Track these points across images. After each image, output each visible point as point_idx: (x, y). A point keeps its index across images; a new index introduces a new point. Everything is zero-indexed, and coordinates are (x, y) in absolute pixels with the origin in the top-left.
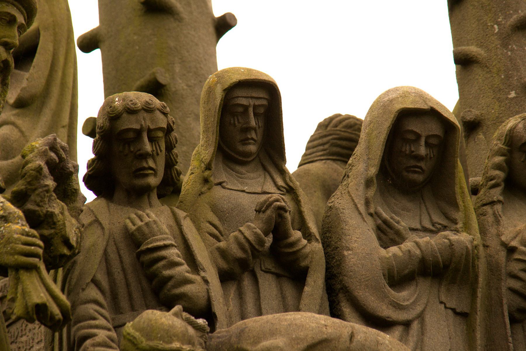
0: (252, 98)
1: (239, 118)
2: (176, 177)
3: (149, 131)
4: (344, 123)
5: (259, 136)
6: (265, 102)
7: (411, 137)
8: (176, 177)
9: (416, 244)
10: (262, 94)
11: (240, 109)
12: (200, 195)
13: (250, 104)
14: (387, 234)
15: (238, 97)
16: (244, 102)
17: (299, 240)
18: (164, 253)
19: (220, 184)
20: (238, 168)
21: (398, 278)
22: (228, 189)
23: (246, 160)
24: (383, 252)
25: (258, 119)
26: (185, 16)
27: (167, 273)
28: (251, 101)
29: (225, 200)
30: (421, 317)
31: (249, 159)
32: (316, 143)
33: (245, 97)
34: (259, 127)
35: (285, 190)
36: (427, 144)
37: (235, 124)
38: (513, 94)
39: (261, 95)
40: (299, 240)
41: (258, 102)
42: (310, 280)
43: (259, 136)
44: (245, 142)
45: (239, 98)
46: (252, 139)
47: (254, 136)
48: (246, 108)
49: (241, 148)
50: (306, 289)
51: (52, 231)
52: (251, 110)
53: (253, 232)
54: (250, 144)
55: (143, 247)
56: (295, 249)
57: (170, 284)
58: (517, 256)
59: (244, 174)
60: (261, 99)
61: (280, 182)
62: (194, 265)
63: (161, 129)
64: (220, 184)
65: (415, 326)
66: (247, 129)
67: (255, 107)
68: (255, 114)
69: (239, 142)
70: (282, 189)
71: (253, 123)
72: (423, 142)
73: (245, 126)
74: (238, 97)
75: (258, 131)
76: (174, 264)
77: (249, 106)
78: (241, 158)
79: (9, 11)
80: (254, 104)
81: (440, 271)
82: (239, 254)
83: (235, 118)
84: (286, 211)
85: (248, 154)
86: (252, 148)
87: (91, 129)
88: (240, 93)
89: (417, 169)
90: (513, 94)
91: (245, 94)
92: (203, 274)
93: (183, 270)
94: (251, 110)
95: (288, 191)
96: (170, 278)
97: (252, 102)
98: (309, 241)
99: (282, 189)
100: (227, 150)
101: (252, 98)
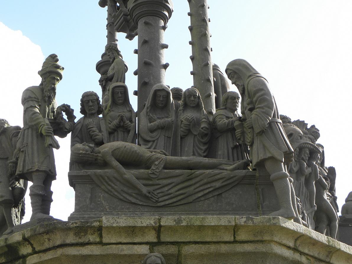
3: (91, 100)
4: (175, 90)
7: (159, 96)
9: (157, 122)
10: (122, 88)
11: (117, 93)
14: (151, 120)
16: (118, 91)
17: (128, 123)
18: (92, 129)
19: (113, 111)
21: (152, 131)
24: (149, 125)
26: (154, 65)
27: (93, 133)
30: (158, 139)
38: (202, 82)
40: (128, 123)
42: (131, 133)
48: (118, 92)
50: (129, 135)
51: (63, 126)
52: (120, 93)
55: (89, 127)
57: (93, 136)
58: (183, 123)
62: (100, 131)
63: (95, 99)
64: (113, 111)
65: (156, 141)
68: (121, 93)
72: (162, 97)
76: (94, 131)
79: (53, 76)
81: (162, 128)
82: (114, 128)
84: (124, 117)
87: (136, 93)
90: (202, 82)
92: (103, 133)
93: (97, 132)
94: (120, 93)
96: (93, 135)
97: (120, 91)
98: (132, 123)
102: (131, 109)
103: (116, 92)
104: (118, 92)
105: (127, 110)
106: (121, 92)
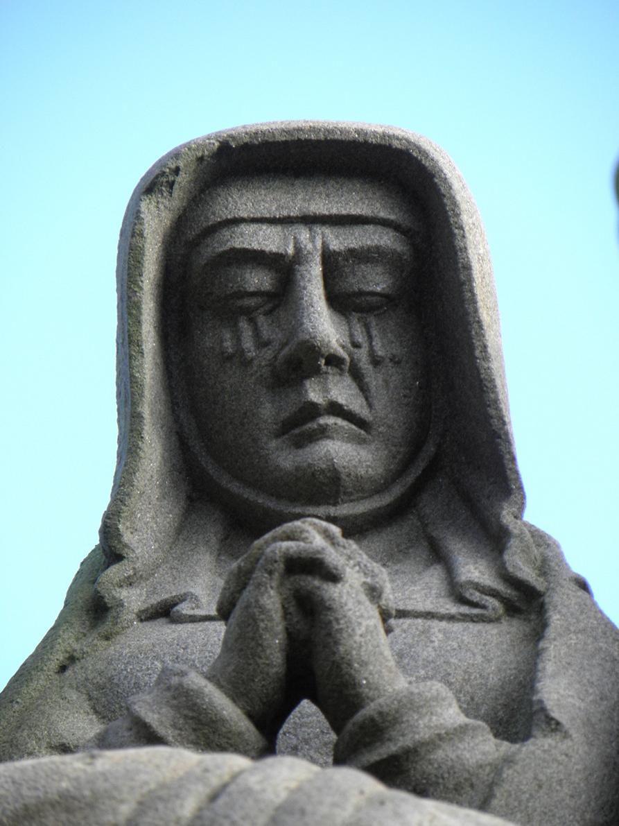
0: (310, 220)
1: (261, 319)
11: (258, 280)
12: (63, 669)
13: (298, 250)
16: (268, 240)
22: (193, 619)
25: (367, 327)
28: (304, 234)
29: (156, 658)
33: (272, 221)
34: (376, 362)
35: (492, 602)
36: (339, 301)
37: (240, 352)
41: (339, 240)
43: (378, 405)
44: (302, 425)
46: (335, 409)
47: (342, 391)
48: (285, 269)
49: (286, 459)
53: (169, 689)
54: (323, 433)
56: (391, 748)
60: (360, 220)
66: (306, 360)
69: (277, 436)
71: (326, 327)
75: (374, 379)
77: (299, 257)
83: (244, 324)
84: (333, 577)
86: (341, 451)
88: (243, 201)
95: (512, 610)
97: (312, 241)
99: (476, 596)
100: (235, 487)
101: (310, 220)
102: (527, 573)
103: (238, 338)
104: (285, 269)
105: (457, 593)
106: (330, 261)
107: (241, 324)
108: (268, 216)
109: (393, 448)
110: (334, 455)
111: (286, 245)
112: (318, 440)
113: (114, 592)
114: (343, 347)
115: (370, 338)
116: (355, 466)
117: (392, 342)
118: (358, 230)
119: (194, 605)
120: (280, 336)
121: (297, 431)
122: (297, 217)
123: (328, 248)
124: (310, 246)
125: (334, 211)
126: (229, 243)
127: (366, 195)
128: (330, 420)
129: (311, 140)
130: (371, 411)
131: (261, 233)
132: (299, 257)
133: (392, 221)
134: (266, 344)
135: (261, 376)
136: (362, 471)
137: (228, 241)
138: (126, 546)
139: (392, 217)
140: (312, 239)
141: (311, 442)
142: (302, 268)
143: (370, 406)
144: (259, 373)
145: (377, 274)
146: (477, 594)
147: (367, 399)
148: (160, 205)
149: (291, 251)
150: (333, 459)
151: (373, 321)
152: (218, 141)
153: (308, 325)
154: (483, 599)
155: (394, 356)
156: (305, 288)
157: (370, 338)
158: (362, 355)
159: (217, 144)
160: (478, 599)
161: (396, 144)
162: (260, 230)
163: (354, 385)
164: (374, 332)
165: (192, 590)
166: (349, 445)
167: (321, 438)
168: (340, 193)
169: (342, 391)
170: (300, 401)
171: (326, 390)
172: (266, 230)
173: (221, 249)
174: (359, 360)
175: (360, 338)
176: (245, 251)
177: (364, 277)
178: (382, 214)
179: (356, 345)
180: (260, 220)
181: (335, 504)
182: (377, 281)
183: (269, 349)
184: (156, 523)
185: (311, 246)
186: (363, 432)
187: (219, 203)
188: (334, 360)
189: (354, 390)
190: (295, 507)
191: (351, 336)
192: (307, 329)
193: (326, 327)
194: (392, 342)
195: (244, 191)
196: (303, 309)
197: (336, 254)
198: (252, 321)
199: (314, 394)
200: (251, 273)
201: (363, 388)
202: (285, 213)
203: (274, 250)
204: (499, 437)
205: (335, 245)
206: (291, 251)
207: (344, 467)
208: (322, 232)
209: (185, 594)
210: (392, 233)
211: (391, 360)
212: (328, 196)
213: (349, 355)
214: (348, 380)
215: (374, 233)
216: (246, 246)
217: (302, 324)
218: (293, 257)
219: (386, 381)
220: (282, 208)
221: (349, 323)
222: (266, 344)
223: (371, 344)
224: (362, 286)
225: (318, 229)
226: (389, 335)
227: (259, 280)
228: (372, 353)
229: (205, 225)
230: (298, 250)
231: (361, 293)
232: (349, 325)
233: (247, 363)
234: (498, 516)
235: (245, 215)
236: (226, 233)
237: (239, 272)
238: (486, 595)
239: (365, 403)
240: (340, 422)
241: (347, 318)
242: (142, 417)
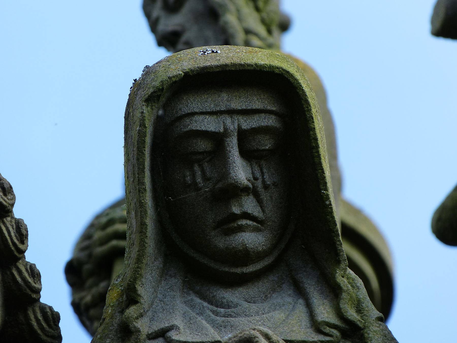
0: (231, 112)
1: (207, 166)
2: (42, 329)
5: (269, 207)
6: (269, 121)
8: (42, 329)
11: (203, 145)
13: (226, 129)
15: (193, 114)
16: (210, 124)
20: (228, 295)
23: (239, 270)
28: (228, 121)
31: (251, 269)
32: (49, 313)
34: (266, 187)
35: (335, 332)
36: (246, 154)
39: (257, 104)
41: (248, 123)
44: (229, 224)
45: (196, 118)
46: (246, 216)
47: (249, 205)
48: (218, 140)
49: (221, 242)
54: (241, 229)
59: (236, 306)
60: (259, 111)
61: (325, 313)
66: (236, 191)
67: (243, 135)
69: (215, 229)
70: (328, 330)
73: (220, 185)
74: (193, 114)
75: (265, 196)
77: (225, 134)
78: (227, 269)
80: (239, 126)
83: (196, 168)
85: (245, 256)
86: (252, 239)
89: (40, 318)
91: (210, 106)
97: (232, 124)
99: (328, 330)
101: (231, 112)
103: (193, 175)
106: (243, 135)
107: (195, 168)
108: (209, 110)
109: (275, 232)
110: (246, 242)
111: (220, 127)
112: (237, 232)
113: (134, 323)
114: (249, 180)
115: (263, 174)
116: (257, 247)
117: (274, 174)
118: (256, 117)
119: (178, 333)
120: (216, 175)
121: (225, 227)
122: (224, 111)
123: (241, 128)
124: (232, 127)
125: (244, 107)
126: (189, 127)
127: (260, 97)
128: (244, 222)
129: (262, 126)
130: (264, 214)
131: (206, 120)
132: (225, 134)
133: (274, 111)
134: (209, 179)
135: (206, 197)
136: (260, 249)
137: (189, 125)
138: (139, 296)
139: (274, 109)
140: (233, 122)
141: (233, 233)
142: (228, 139)
143: (263, 211)
144: (205, 196)
145: (266, 140)
146: (328, 328)
147: (261, 207)
148: (153, 107)
149: (222, 130)
150: (246, 245)
151: (263, 162)
152: (183, 72)
153: (233, 174)
154: (330, 331)
155: (275, 182)
156: (230, 152)
157: (263, 174)
158: (259, 184)
159: (183, 74)
160: (328, 331)
161: (277, 71)
162: (205, 118)
163: (254, 200)
164: (265, 170)
165: (176, 323)
166: (253, 234)
167: (239, 232)
168: (246, 96)
169: (249, 205)
170: (228, 212)
171: (241, 206)
172: (208, 118)
173: (185, 130)
174: (257, 187)
175: (258, 175)
176: (198, 131)
177: (260, 142)
178: (269, 108)
179: (256, 179)
180: (205, 116)
181: (246, 265)
182: (266, 143)
183: (210, 182)
184: (152, 277)
185: (232, 127)
186: (259, 226)
187: (183, 103)
188: (245, 190)
189: (255, 203)
190: (225, 267)
191: (253, 173)
192: (233, 177)
193: (241, 172)
194: (274, 174)
195: (196, 96)
196: (230, 164)
197: (245, 130)
198: (201, 166)
199: (236, 210)
200: (201, 142)
201: (260, 201)
202: (218, 109)
203: (213, 130)
204: (334, 232)
205: (245, 126)
206: (222, 130)
207: (251, 249)
208: (238, 119)
209: (173, 326)
210: (274, 117)
211: (273, 185)
212: (240, 97)
213: (252, 185)
214: (251, 197)
215: (265, 119)
216: (198, 128)
217: (230, 173)
218: (223, 133)
219: (271, 197)
220: (217, 106)
221: (251, 165)
222: (209, 179)
223: (263, 176)
224: (258, 147)
225: (235, 117)
226: (272, 170)
227: (204, 145)
228: (264, 182)
229: (176, 116)
230: (226, 129)
231: (258, 150)
232: (251, 166)
233: (197, 189)
234: (334, 278)
235: (197, 110)
236: (187, 121)
237: (194, 141)
238: (332, 328)
239: (260, 209)
240: (249, 222)
241: (250, 162)
242: (146, 224)
